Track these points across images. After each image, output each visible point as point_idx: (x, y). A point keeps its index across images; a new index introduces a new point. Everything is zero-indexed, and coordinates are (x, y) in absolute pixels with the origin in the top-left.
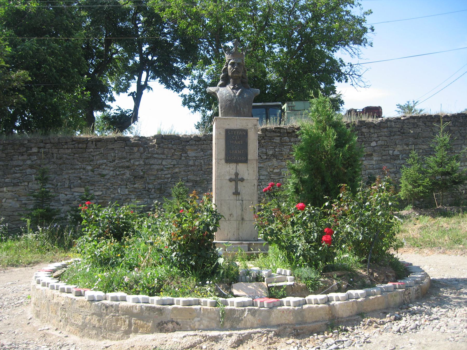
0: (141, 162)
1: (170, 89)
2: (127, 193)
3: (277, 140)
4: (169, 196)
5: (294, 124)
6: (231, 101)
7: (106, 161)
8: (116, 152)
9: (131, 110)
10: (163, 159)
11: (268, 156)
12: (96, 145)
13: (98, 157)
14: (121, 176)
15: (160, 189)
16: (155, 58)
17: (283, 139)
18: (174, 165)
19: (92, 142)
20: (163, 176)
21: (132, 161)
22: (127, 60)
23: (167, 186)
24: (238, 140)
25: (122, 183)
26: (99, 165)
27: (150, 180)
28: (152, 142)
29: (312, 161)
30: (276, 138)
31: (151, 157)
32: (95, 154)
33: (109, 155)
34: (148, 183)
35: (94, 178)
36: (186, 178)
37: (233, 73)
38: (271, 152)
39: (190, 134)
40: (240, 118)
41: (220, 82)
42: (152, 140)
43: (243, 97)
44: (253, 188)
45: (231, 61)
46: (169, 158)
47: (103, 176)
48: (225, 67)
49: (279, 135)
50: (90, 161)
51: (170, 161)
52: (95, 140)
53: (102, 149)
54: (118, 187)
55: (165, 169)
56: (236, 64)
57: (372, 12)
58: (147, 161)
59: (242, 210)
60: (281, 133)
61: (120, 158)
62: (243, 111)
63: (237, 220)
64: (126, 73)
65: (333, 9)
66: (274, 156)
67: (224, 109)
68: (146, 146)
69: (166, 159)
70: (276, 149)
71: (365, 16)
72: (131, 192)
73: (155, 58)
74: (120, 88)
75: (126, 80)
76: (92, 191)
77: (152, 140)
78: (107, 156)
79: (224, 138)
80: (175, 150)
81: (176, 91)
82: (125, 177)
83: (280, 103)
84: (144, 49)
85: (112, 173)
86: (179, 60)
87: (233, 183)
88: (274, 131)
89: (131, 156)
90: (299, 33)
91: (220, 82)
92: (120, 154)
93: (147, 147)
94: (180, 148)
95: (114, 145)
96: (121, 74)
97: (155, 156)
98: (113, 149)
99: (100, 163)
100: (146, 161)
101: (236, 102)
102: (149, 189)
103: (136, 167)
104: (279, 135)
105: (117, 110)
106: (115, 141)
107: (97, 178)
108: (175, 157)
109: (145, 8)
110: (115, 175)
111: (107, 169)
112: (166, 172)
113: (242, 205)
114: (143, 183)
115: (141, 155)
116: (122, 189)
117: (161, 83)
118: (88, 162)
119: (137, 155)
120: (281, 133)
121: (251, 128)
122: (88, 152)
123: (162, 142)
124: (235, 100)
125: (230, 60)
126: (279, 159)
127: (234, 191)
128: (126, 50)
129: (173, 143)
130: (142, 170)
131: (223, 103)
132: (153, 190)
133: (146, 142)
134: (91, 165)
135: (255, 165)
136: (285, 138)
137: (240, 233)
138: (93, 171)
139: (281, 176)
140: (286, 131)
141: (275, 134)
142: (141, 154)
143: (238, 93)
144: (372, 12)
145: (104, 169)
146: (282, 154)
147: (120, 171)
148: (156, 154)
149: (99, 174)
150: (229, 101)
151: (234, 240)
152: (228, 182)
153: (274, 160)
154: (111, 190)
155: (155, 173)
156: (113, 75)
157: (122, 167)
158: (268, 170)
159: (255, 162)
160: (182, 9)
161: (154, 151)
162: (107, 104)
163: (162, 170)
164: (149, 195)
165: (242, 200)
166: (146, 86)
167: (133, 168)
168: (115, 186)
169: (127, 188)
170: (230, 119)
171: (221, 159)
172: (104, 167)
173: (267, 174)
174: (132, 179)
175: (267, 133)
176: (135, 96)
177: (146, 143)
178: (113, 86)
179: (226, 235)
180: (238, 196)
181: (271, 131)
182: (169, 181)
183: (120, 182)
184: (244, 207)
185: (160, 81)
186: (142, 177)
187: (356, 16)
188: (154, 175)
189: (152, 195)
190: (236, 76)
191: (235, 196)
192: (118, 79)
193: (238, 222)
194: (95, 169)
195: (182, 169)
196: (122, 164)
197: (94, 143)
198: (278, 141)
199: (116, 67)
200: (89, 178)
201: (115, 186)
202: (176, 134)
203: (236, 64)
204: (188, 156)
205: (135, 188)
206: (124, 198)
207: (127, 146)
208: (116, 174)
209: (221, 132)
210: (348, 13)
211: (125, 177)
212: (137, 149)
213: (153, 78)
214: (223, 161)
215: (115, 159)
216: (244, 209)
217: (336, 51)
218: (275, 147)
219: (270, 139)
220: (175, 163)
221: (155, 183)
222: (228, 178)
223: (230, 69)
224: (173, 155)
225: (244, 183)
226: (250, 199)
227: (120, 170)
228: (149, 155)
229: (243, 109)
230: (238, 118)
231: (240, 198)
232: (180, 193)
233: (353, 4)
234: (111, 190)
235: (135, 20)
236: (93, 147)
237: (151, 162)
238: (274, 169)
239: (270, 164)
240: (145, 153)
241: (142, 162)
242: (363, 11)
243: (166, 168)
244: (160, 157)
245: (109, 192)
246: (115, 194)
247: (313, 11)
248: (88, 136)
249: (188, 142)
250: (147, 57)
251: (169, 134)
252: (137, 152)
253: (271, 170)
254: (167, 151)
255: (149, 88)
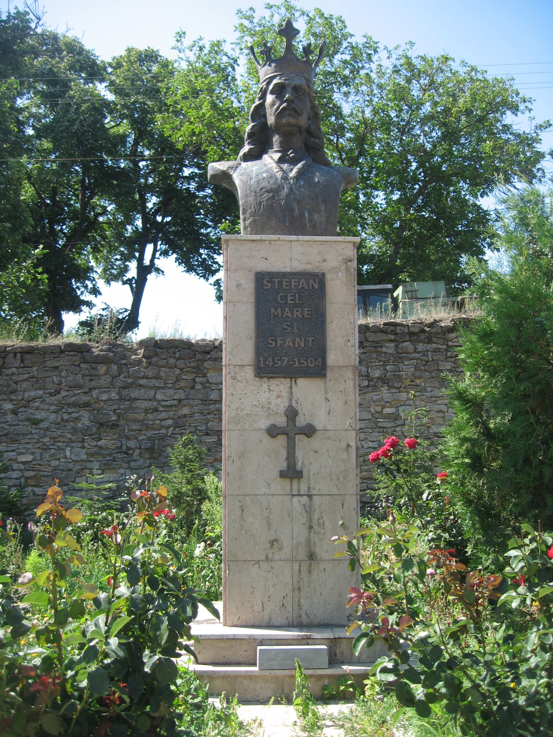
0: (113, 395)
1: (194, 273)
2: (84, 457)
3: (390, 348)
4: (165, 466)
5: (422, 316)
6: (275, 191)
7: (41, 392)
8: (63, 375)
9: (126, 310)
10: (158, 388)
11: (372, 380)
12: (22, 361)
13: (25, 385)
14: (72, 424)
15: (151, 450)
16: (169, 219)
17: (400, 346)
18: (180, 401)
19: (15, 354)
20: (158, 422)
21: (95, 393)
22: (123, 225)
23: (164, 444)
24: (296, 305)
25: (73, 438)
26: (29, 401)
27: (131, 430)
28: (136, 354)
29: (524, 369)
30: (387, 344)
31: (132, 383)
32: (21, 377)
33: (48, 379)
34: (128, 438)
35: (17, 427)
36: (204, 428)
37: (279, 115)
38: (377, 374)
39: (212, 339)
40: (301, 238)
41: (246, 148)
42: (137, 350)
43: (310, 183)
44: (345, 456)
45: (275, 81)
46: (170, 385)
47: (36, 422)
48: (257, 102)
49: (393, 337)
50: (11, 393)
51: (172, 392)
52: (20, 350)
53: (35, 368)
54: (67, 446)
55: (161, 409)
56: (289, 89)
57: (550, 125)
58: (125, 392)
59: (311, 527)
60: (396, 334)
61: (70, 387)
62: (311, 220)
63: (292, 560)
64: (122, 249)
65: (482, 119)
66: (383, 380)
67: (253, 215)
68: (123, 362)
69: (163, 388)
70: (388, 368)
71: (539, 131)
72: (92, 455)
73: (169, 219)
74: (112, 274)
75: (121, 260)
76: (13, 453)
77: (137, 350)
78: (44, 382)
79: (252, 299)
80: (181, 369)
81: (204, 276)
82: (80, 425)
83: (390, 286)
84: (150, 205)
85: (53, 416)
86: (210, 223)
87: (282, 440)
88: (382, 331)
89: (93, 383)
90: (421, 164)
91: (246, 148)
92: (70, 379)
93: (125, 364)
94: (192, 365)
95: (58, 361)
96: (112, 250)
97: (142, 382)
98: (56, 368)
99: (29, 397)
100: (123, 393)
101: (288, 195)
102: (129, 449)
103: (102, 404)
104: (393, 337)
105: (103, 309)
106: (62, 352)
107: (23, 428)
108: (183, 384)
109: (151, 134)
110: (59, 420)
111: (42, 410)
112: (163, 415)
113: (309, 510)
114: (116, 436)
115: (112, 381)
116: (75, 450)
117: (180, 264)
118: (6, 394)
119: (105, 381)
120: (396, 334)
121: (335, 269)
122: (7, 375)
123: (157, 354)
124: (286, 190)
125: (271, 79)
126: (394, 388)
127: (284, 466)
128: (119, 208)
129: (177, 355)
130: (115, 410)
131: (251, 199)
132: (137, 452)
133: (125, 355)
134: (11, 400)
135: (350, 383)
136: (404, 344)
137: (302, 601)
138: (15, 412)
139: (399, 422)
140: (406, 330)
141: (384, 337)
142: (113, 377)
143: (295, 170)
144: (550, 125)
145: (37, 409)
146: (399, 376)
147: (70, 413)
148: (143, 378)
149: (28, 419)
150: (268, 191)
151: (284, 622)
152: (266, 438)
153: (385, 389)
154: (53, 451)
155: (141, 416)
156: (99, 251)
157: (75, 405)
158: (372, 410)
159: (349, 374)
160: (210, 126)
161: (139, 371)
162: (82, 298)
163: (156, 410)
164: (128, 462)
165: (310, 496)
166: (152, 268)
167: (96, 406)
168: (60, 444)
169: (83, 447)
170: (270, 241)
171: (242, 366)
172: (37, 404)
173: (370, 417)
174: (94, 430)
175: (368, 334)
176: (134, 285)
177: (124, 357)
178: (99, 270)
179: (258, 608)
180: (295, 482)
181: (376, 330)
182: (169, 434)
183: (69, 436)
184: (316, 516)
185: (177, 259)
186: (115, 426)
187: (521, 133)
188: (139, 421)
189: (134, 461)
190: (290, 125)
191: (288, 481)
192: (107, 260)
193: (296, 566)
194: (21, 410)
195: (196, 409)
196: (73, 399)
197: (19, 355)
198: (391, 351)
199: (104, 238)
200: (6, 427)
201: (60, 444)
202: (185, 337)
203: (289, 89)
204: (208, 381)
205: (101, 448)
206: (78, 467)
207: (84, 362)
208: (63, 420)
209: (243, 281)
210: (507, 128)
211: (80, 425)
212: (105, 368)
213: (165, 253)
214: (249, 372)
215: (61, 389)
216: (315, 523)
217: (487, 195)
218: (385, 362)
219: (375, 347)
220: (183, 397)
221: (140, 438)
222: (264, 424)
223: (273, 104)
224: (177, 380)
225: (315, 442)
226: (335, 491)
227: (70, 410)
228: (130, 381)
229: (310, 214)
230: (294, 237)
231: (304, 489)
232: (187, 459)
233: (517, 110)
234: (53, 451)
235: (135, 157)
236: (17, 365)
237: (134, 395)
238: (383, 407)
239: (375, 398)
240: (123, 375)
241: (114, 395)
242: (534, 123)
243: (163, 406)
244: (151, 385)
245: (47, 456)
246: (58, 459)
247: (445, 124)
248: (9, 343)
249: (208, 353)
250: (155, 217)
251: (172, 338)
252: (105, 374)
253: (378, 409)
254: (166, 372)
255: (158, 270)
